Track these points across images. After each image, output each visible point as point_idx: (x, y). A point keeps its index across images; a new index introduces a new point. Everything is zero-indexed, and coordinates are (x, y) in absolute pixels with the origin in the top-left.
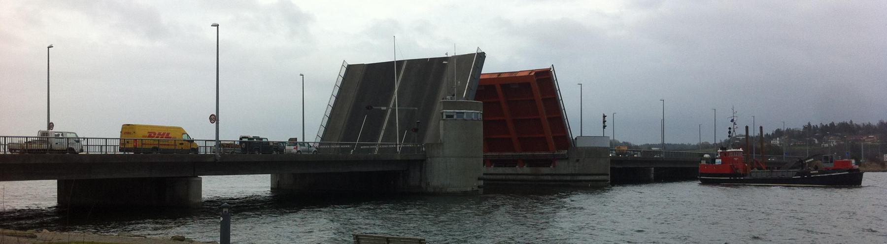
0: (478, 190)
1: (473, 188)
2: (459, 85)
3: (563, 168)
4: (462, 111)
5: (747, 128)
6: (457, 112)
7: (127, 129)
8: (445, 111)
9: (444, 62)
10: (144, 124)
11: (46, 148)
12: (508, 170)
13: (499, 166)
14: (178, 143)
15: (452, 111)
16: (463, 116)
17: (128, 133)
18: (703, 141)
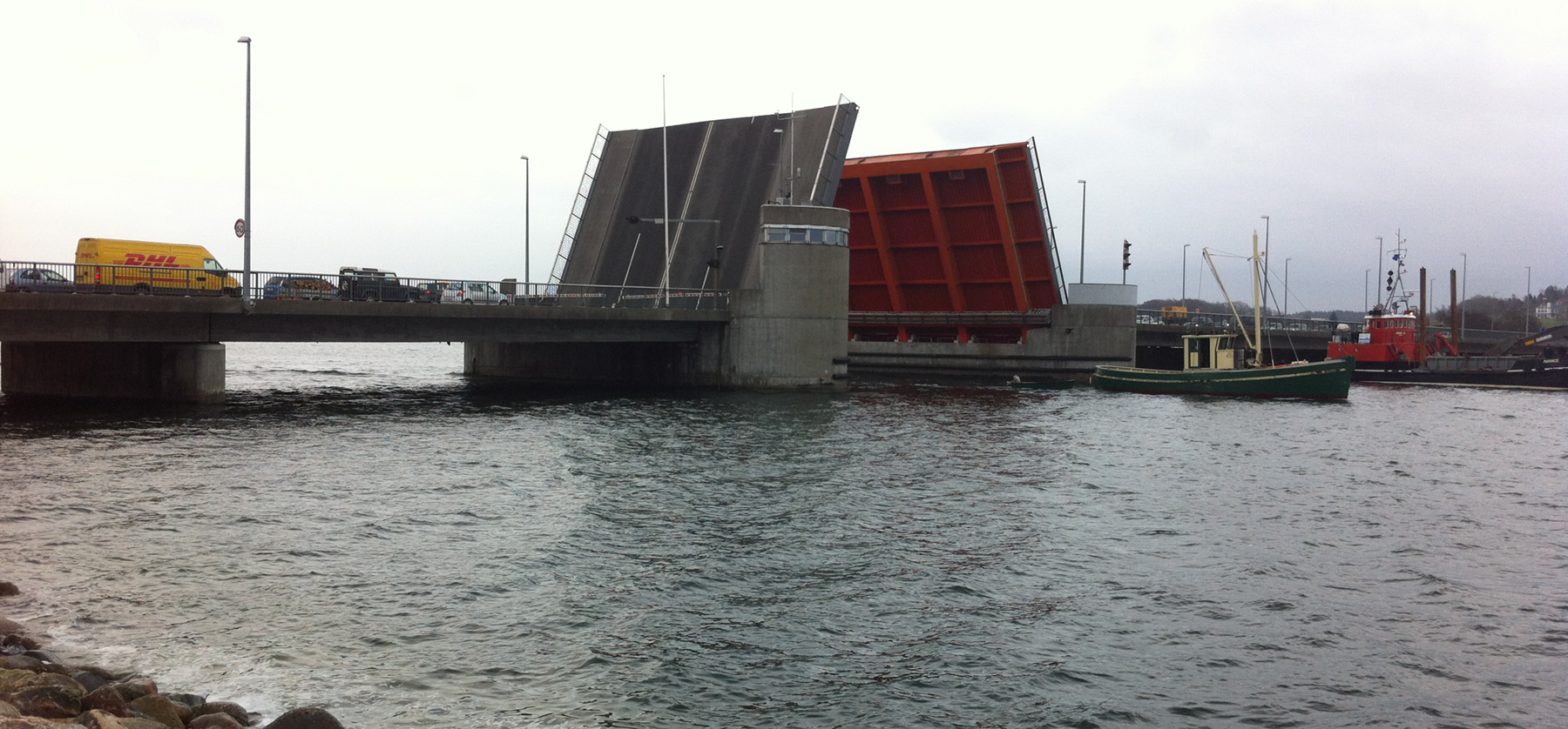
0: (831, 384)
1: (821, 380)
2: (799, 175)
3: (1040, 344)
4: (803, 227)
5: (1453, 273)
6: (791, 229)
7: (88, 248)
8: (766, 226)
9: (776, 131)
10: (120, 238)
11: (111, 284)
12: (940, 348)
13: (924, 341)
14: (193, 276)
15: (781, 226)
16: (804, 236)
17: (87, 256)
18: (1192, 295)
